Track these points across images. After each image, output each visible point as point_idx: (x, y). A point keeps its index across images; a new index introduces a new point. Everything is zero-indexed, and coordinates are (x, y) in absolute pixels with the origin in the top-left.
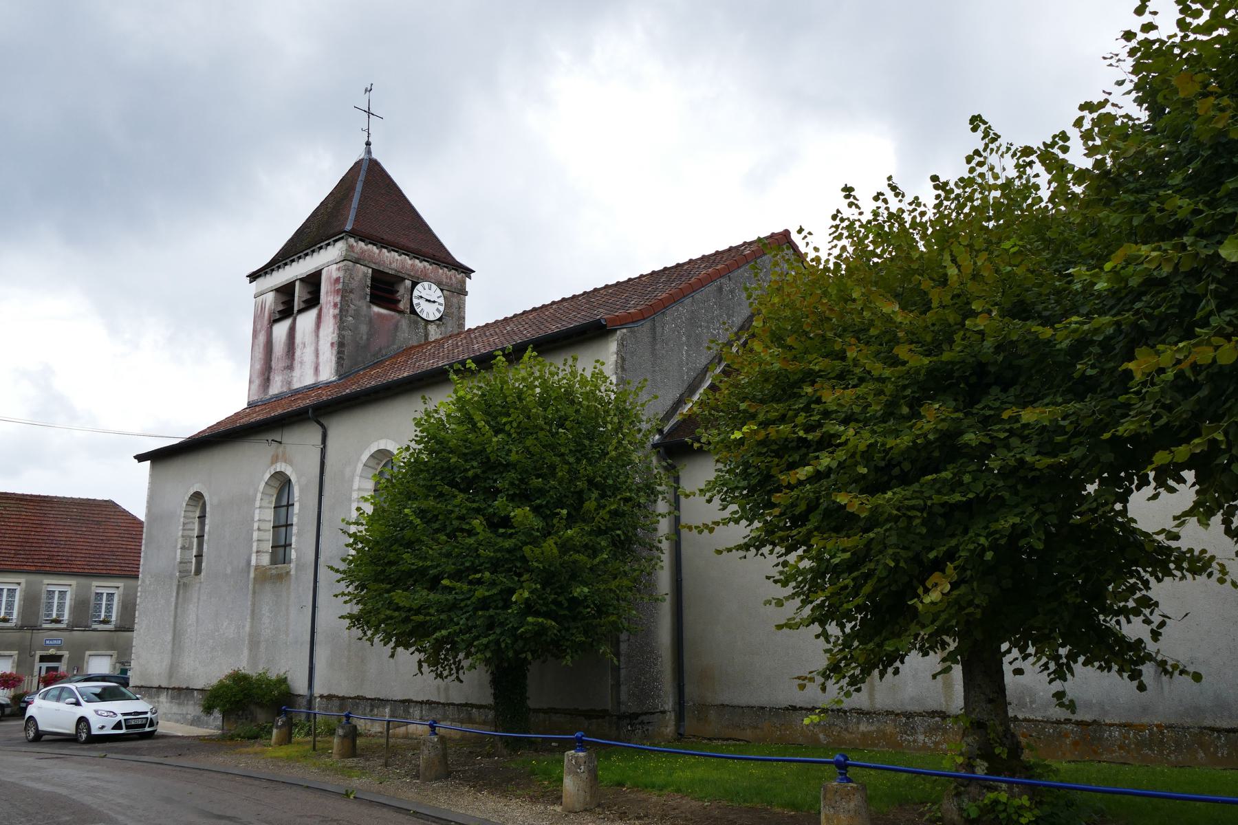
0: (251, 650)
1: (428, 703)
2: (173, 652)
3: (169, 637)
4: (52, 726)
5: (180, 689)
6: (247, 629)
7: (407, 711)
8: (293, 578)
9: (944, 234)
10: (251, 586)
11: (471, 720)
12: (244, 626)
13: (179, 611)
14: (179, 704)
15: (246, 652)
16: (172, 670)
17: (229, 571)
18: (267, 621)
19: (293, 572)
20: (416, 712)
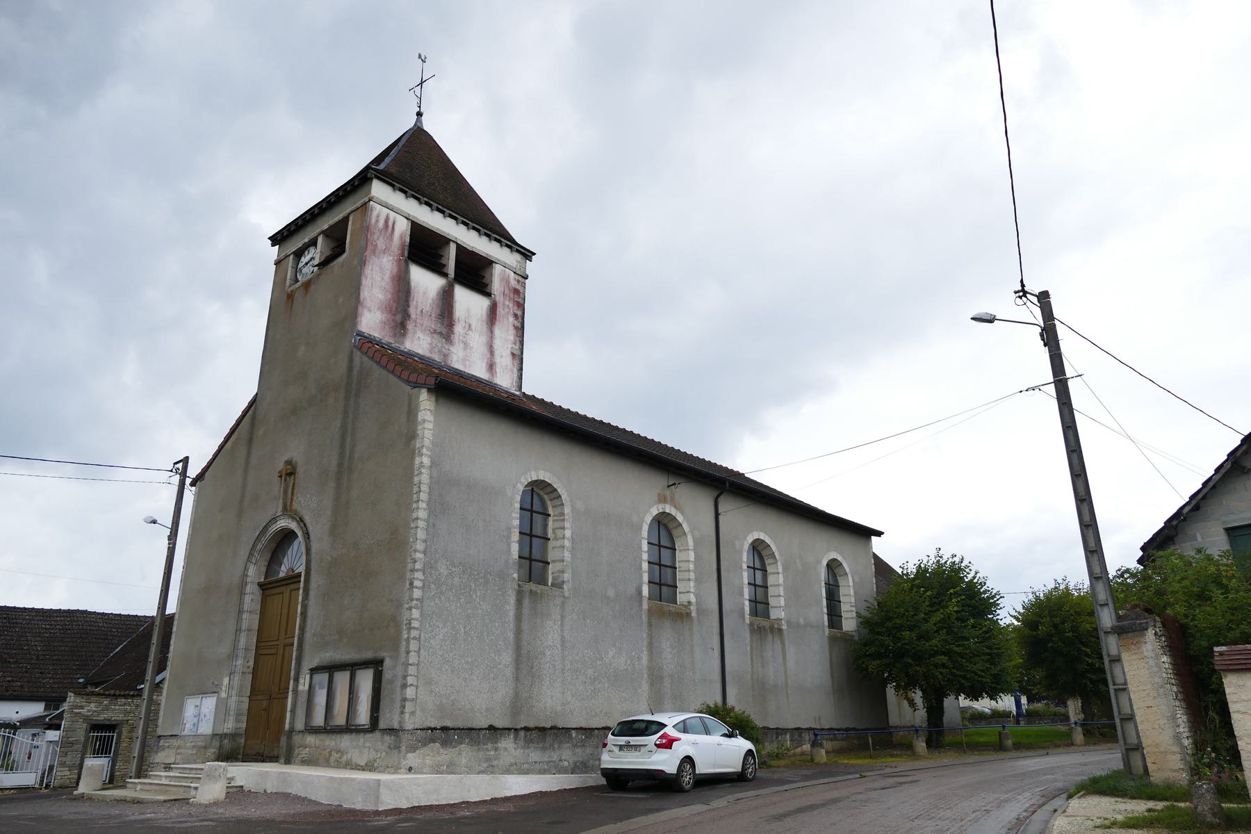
0: (652, 685)
1: (581, 728)
2: (517, 679)
3: (507, 658)
4: (715, 766)
5: (542, 730)
6: (645, 660)
7: (800, 735)
8: (695, 620)
9: (935, 573)
10: (645, 618)
11: (835, 739)
12: (639, 659)
13: (525, 626)
14: (544, 749)
15: (645, 686)
16: (517, 704)
17: (611, 593)
18: (670, 657)
19: (694, 614)
20: (806, 736)
